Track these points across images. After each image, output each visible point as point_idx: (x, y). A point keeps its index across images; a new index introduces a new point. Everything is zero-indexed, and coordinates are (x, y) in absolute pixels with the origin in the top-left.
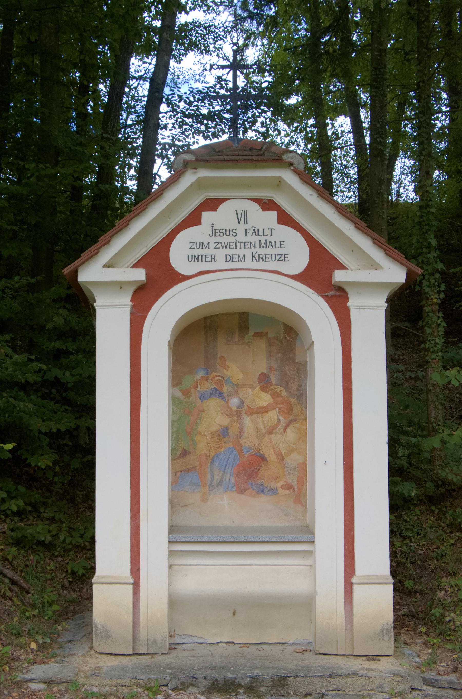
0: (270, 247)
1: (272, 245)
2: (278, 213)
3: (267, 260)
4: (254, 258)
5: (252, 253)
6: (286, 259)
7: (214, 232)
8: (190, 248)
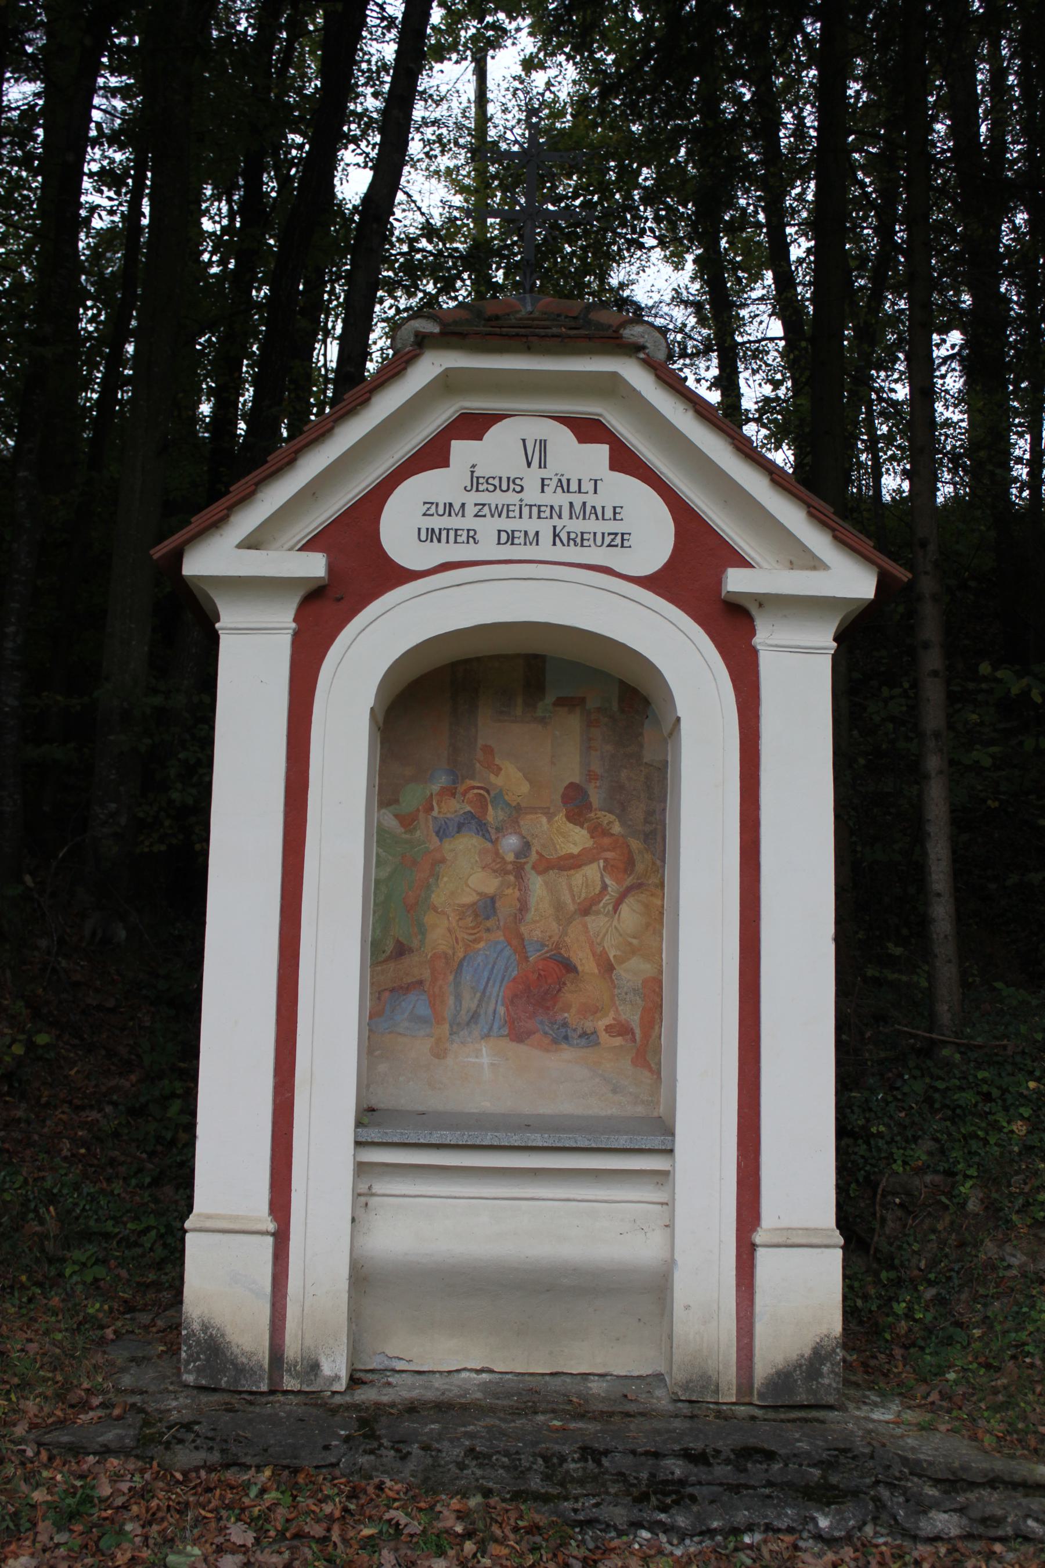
0: (593, 516)
2: (611, 450)
3: (586, 543)
5: (555, 527)
6: (626, 543)
8: (424, 515)
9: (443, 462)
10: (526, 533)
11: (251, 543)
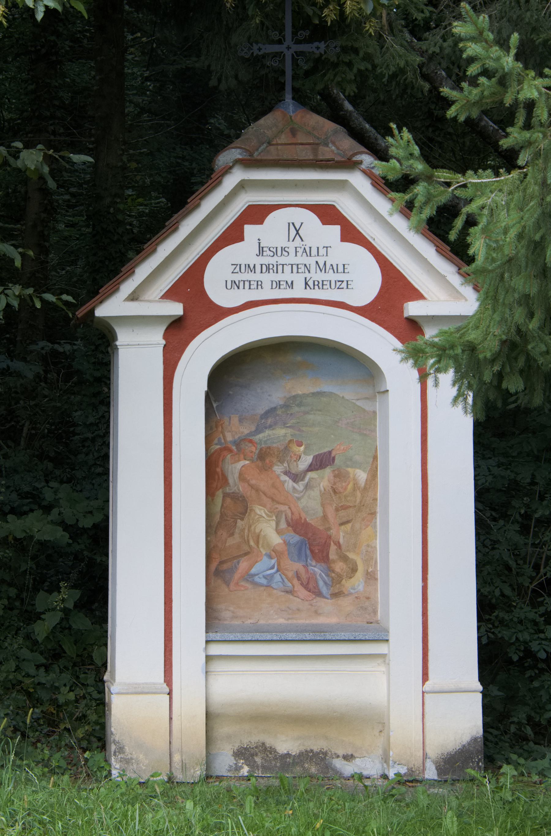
0: (331, 271)
1: (335, 269)
2: (246, 224)
3: (324, 287)
4: (307, 286)
5: (306, 278)
7: (261, 251)
8: (232, 273)
9: (241, 238)
10: (287, 282)
11: (133, 297)
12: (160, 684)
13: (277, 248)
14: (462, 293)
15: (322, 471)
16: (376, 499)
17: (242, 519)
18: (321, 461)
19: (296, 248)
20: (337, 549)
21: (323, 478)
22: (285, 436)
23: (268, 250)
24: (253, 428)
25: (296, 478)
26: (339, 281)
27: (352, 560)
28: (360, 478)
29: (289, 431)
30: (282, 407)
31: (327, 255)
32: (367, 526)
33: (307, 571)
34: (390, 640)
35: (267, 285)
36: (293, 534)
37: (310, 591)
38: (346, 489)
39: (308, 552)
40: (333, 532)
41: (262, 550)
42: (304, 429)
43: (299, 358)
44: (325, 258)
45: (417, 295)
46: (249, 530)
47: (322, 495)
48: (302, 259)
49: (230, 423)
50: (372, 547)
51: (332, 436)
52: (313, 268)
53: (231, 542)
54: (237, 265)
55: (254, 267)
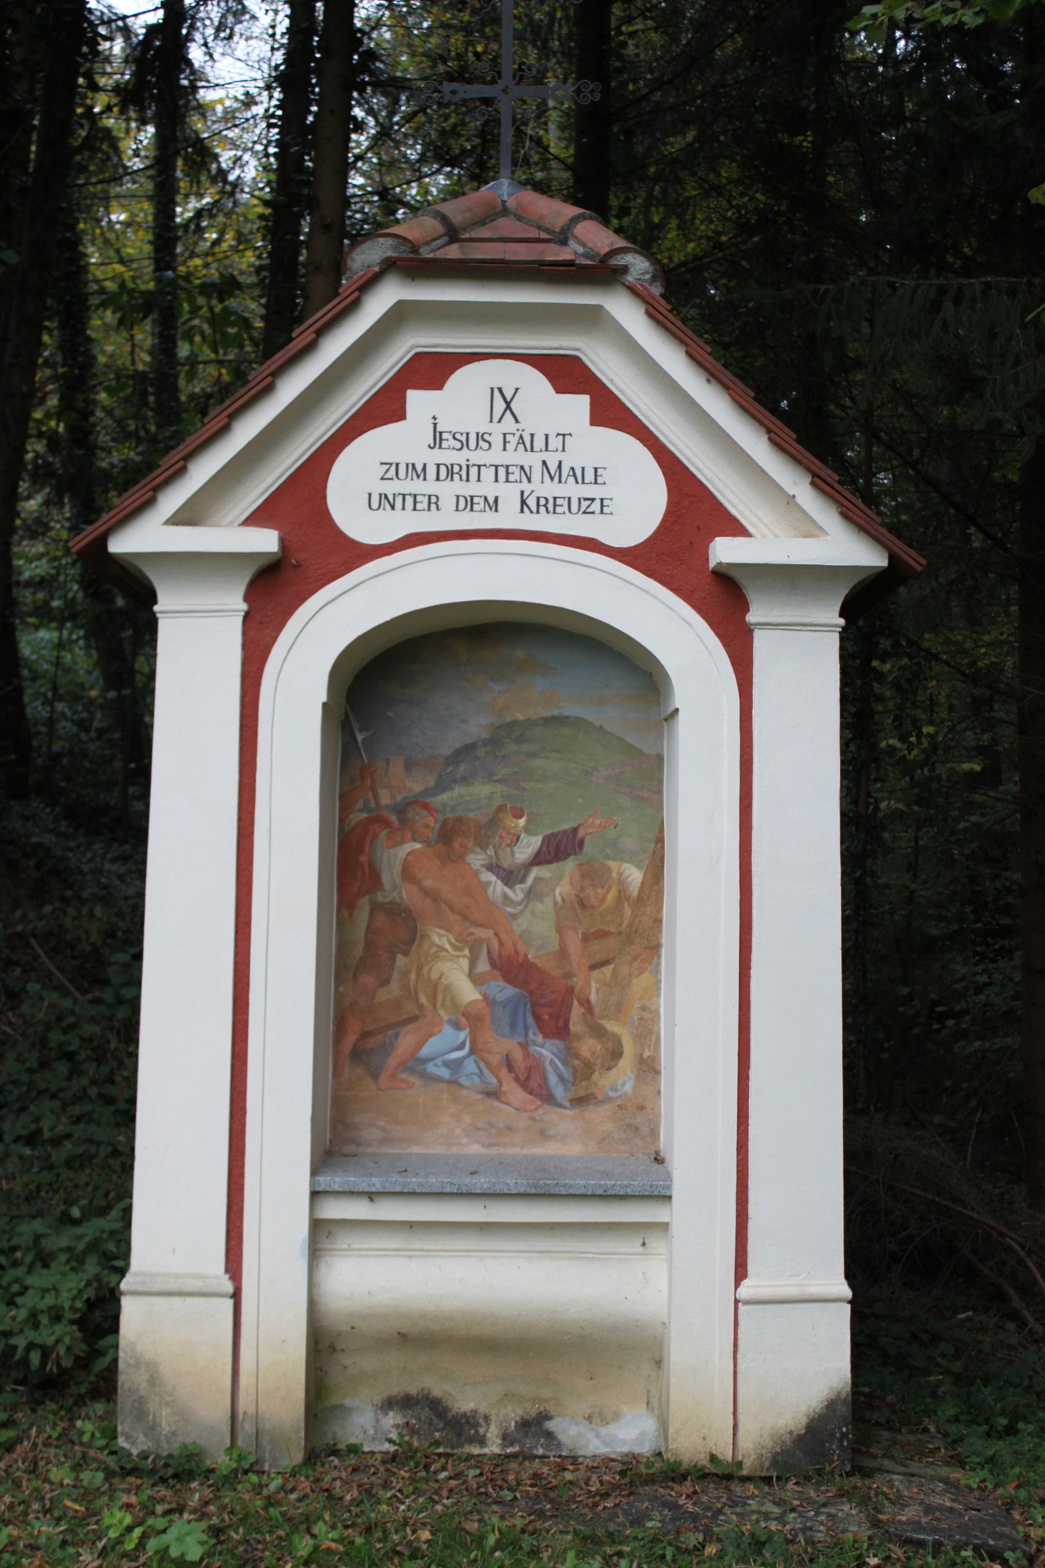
0: (572, 479)
1: (578, 476)
2: (591, 398)
3: (559, 509)
4: (525, 508)
5: (522, 493)
7: (438, 439)
8: (382, 479)
11: (178, 519)
12: (216, 1277)
13: (468, 434)
14: (821, 524)
15: (560, 864)
16: (660, 921)
17: (406, 953)
18: (558, 846)
19: (505, 435)
20: (584, 1014)
21: (560, 878)
22: (491, 798)
23: (450, 437)
24: (431, 782)
25: (510, 877)
26: (586, 499)
27: (614, 1034)
28: (630, 879)
29: (499, 788)
30: (486, 743)
31: (564, 450)
32: (641, 971)
33: (527, 1055)
34: (674, 1198)
35: (448, 503)
36: (502, 984)
37: (531, 1093)
38: (603, 900)
39: (530, 1020)
40: (578, 981)
41: (442, 1012)
42: (526, 785)
43: (520, 653)
44: (560, 456)
45: (736, 529)
46: (419, 973)
47: (558, 910)
48: (516, 457)
49: (387, 771)
50: (651, 1012)
51: (580, 800)
52: (537, 473)
53: (384, 995)
54: (391, 464)
55: (424, 469)
